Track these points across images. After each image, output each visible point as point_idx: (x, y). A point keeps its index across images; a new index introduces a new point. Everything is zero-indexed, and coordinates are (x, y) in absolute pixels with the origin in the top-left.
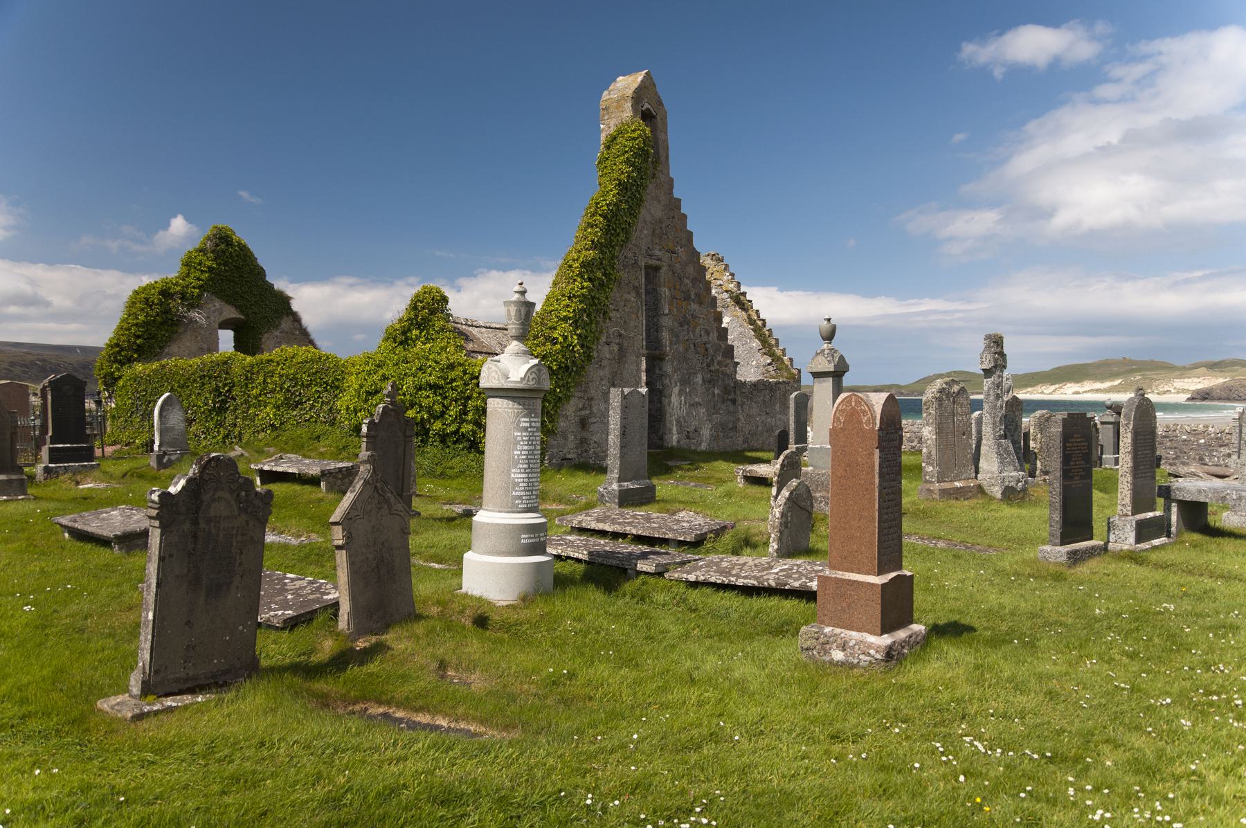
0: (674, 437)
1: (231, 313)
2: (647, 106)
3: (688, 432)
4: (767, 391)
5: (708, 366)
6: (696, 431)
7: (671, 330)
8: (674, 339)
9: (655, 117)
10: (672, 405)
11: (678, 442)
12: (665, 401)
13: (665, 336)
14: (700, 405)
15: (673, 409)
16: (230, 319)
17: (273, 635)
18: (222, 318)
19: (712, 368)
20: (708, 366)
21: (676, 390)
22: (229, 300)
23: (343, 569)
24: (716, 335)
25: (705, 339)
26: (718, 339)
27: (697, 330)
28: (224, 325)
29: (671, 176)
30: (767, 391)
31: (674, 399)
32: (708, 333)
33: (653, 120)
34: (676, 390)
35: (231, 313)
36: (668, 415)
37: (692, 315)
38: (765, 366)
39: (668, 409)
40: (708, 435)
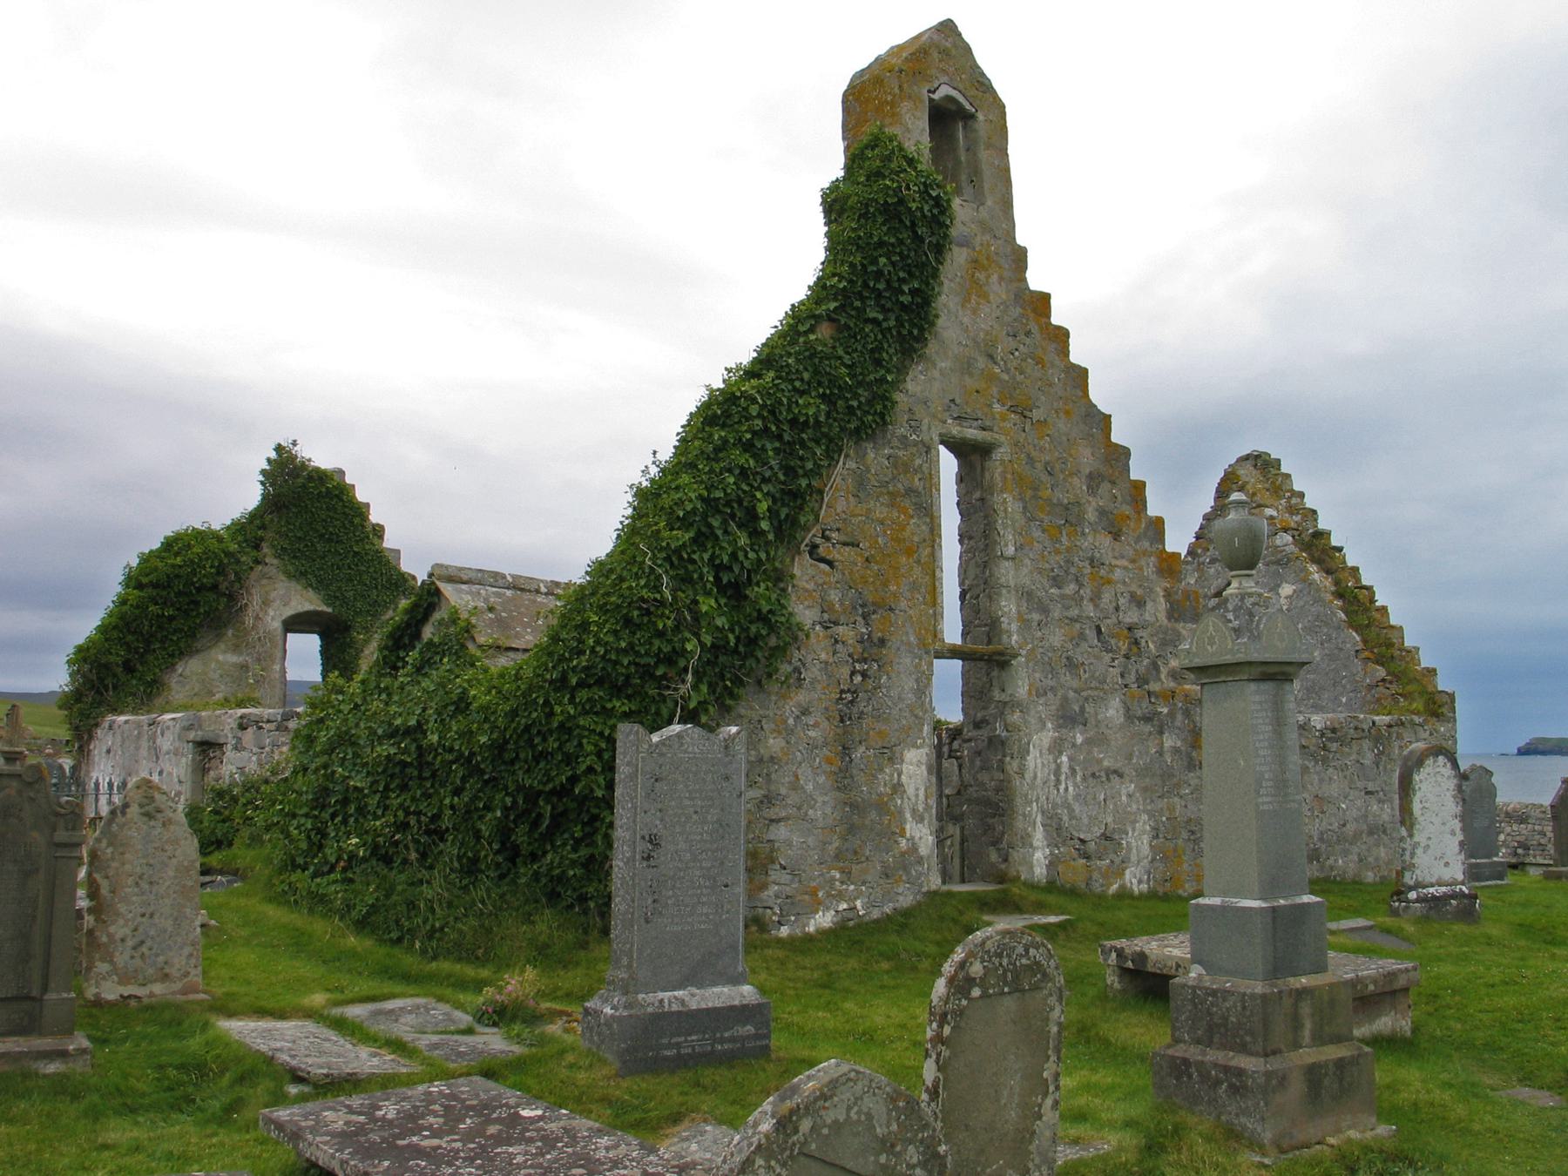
0: (1038, 855)
1: (306, 601)
2: (944, 91)
3: (1082, 841)
4: (1366, 744)
5: (1142, 681)
6: (1106, 837)
7: (1027, 595)
8: (1036, 616)
9: (972, 117)
10: (1028, 776)
11: (1051, 865)
12: (1012, 766)
13: (1008, 607)
14: (1121, 776)
15: (1032, 786)
16: (308, 613)
17: (1447, 771)
18: (289, 612)
19: (1154, 686)
20: (1142, 681)
21: (1043, 738)
22: (319, 584)
23: (272, 1112)
24: (1162, 604)
25: (1131, 617)
26: (1169, 618)
27: (1107, 597)
28: (297, 624)
29: (1021, 239)
30: (1366, 744)
31: (1036, 761)
32: (1140, 603)
33: (970, 123)
34: (1043, 738)
35: (306, 601)
36: (1019, 801)
37: (1092, 560)
38: (1370, 687)
39: (1020, 786)
40: (1146, 850)
